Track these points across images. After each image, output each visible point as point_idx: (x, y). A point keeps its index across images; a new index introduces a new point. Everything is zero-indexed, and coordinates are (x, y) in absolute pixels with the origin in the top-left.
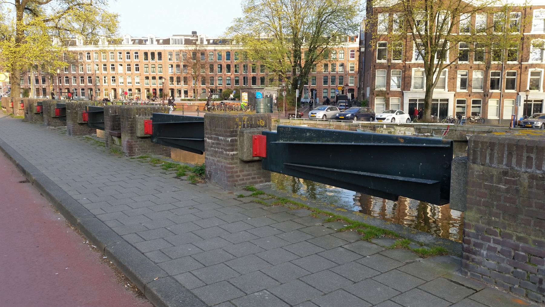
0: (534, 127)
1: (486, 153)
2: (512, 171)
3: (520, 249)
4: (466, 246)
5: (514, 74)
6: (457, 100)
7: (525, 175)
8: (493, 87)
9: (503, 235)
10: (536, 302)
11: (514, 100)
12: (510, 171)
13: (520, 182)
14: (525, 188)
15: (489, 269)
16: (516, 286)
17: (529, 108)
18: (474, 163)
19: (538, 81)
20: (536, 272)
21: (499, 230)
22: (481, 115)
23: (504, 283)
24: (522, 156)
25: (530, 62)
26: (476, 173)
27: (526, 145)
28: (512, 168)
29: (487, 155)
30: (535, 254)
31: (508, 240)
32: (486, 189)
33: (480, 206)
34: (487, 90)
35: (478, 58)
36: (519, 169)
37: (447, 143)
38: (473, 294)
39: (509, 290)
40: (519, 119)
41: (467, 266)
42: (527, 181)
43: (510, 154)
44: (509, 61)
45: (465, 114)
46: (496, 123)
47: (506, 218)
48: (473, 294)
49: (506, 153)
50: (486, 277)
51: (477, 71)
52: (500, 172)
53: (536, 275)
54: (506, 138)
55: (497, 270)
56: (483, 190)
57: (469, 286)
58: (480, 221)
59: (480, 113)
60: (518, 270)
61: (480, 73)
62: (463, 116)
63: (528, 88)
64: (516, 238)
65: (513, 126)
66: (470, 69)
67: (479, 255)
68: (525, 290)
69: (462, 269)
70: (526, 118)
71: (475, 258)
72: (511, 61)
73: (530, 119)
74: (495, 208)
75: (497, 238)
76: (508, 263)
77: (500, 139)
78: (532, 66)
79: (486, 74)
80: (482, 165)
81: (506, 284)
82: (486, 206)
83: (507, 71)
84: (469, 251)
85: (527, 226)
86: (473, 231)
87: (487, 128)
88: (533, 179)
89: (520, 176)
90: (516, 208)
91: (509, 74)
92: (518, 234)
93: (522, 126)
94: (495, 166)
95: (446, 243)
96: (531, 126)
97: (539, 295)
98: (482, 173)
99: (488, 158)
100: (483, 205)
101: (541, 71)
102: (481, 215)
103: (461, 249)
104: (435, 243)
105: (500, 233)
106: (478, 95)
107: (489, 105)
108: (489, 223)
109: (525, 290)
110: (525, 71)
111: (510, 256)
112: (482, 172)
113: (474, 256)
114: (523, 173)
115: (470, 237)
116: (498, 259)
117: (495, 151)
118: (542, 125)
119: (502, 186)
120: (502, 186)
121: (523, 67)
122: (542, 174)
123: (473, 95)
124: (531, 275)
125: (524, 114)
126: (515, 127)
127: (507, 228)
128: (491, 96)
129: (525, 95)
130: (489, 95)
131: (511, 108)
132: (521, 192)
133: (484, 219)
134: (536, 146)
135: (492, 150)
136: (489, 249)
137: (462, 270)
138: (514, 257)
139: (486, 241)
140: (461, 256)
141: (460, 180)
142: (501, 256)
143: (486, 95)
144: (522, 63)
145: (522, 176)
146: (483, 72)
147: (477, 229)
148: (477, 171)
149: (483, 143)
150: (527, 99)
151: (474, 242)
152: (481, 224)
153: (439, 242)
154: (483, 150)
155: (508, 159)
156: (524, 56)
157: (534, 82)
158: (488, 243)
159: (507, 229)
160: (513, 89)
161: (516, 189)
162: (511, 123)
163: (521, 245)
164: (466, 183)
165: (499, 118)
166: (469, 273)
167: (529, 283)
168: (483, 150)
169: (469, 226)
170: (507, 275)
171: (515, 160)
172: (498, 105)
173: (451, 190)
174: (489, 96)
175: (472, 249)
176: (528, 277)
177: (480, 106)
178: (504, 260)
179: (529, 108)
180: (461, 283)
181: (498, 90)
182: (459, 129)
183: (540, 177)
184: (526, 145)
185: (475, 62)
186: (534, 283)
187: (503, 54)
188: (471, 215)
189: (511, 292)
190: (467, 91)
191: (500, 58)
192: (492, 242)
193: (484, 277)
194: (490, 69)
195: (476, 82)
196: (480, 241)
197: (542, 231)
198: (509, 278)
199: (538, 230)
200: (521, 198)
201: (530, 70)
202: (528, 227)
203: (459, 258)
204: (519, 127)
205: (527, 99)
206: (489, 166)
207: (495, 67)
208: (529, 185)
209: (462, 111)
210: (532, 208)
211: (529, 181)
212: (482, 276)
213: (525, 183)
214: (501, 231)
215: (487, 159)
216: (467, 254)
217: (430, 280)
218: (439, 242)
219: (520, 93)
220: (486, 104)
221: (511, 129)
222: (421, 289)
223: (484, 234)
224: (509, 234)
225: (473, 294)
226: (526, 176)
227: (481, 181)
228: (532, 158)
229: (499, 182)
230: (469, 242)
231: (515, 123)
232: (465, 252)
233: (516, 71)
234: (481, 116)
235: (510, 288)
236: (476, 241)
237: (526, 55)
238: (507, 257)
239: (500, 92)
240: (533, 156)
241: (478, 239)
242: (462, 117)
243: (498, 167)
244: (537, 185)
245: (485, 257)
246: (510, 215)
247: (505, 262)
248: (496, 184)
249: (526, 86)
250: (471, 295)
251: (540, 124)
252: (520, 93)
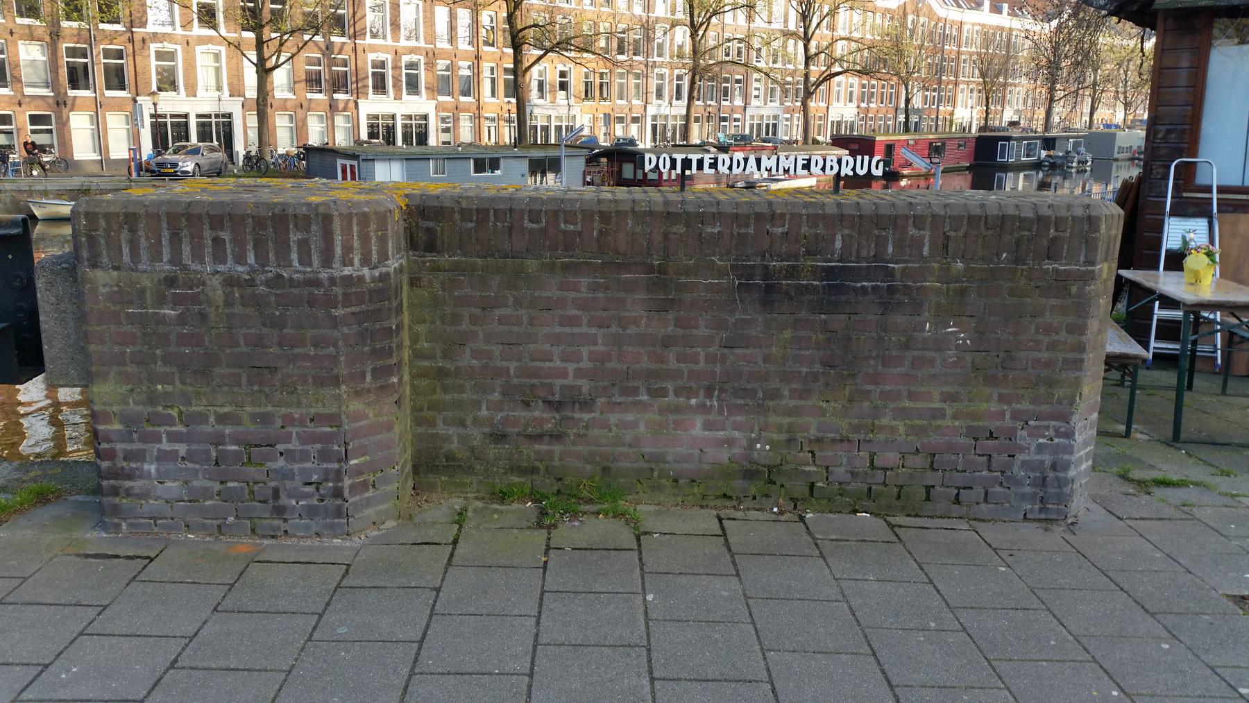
0: (179, 173)
1: (119, 241)
2: (186, 274)
3: (227, 439)
4: (105, 465)
5: (119, 55)
6: (30, 116)
7: (214, 280)
8: (74, 84)
9: (186, 419)
10: (273, 537)
11: (128, 113)
12: (181, 276)
13: (207, 295)
14: (218, 307)
15: (167, 502)
16: (231, 519)
17: (163, 131)
18: (95, 265)
19: (172, 71)
20: (264, 478)
21: (176, 410)
22: (56, 151)
23: (205, 521)
24: (201, 238)
25: (150, 28)
26: (102, 290)
27: (207, 213)
28: (185, 268)
29: (124, 245)
30: (258, 443)
31: (199, 428)
32: (132, 324)
33: (125, 364)
34: (62, 91)
35: (26, 9)
36: (199, 268)
37: (14, 224)
38: (145, 567)
39: (216, 533)
40: (145, 158)
41: (116, 510)
42: (220, 292)
43: (175, 238)
44: (103, 22)
45: (17, 149)
46: (96, 169)
47: (188, 380)
48: (145, 567)
49: (166, 235)
50: (165, 521)
51: (28, 42)
52: (159, 280)
53: (265, 484)
54: (159, 201)
55: (186, 499)
56: (127, 328)
57: (131, 554)
58: (131, 401)
59: (54, 147)
60: (230, 484)
61: (38, 47)
62: (10, 156)
63: (154, 88)
64: (215, 420)
65: (134, 174)
66: (9, 37)
67: (141, 477)
68: (249, 522)
69: (107, 520)
70: (159, 154)
71: (132, 488)
72: (108, 22)
73: (169, 157)
74: (159, 363)
75: (174, 429)
76: (207, 476)
77: (147, 203)
78: (155, 37)
79: (52, 51)
80: (115, 268)
81: (210, 521)
82: (138, 364)
83: (102, 47)
84: (116, 474)
85: (234, 388)
86: (116, 426)
87: (75, 182)
88: (232, 286)
89: (204, 284)
90: (206, 353)
91: (107, 53)
92: (218, 409)
93: (154, 172)
94: (145, 267)
95: (50, 469)
96: (172, 171)
97: (277, 522)
98: (116, 289)
99: (126, 251)
100: (131, 363)
101: (220, 51)
102: (130, 387)
103: (95, 474)
104: (20, 478)
105: (179, 417)
106: (40, 102)
107: (72, 127)
108: (152, 400)
109: (249, 522)
110: (143, 48)
111: (208, 459)
112: (118, 286)
113: (128, 484)
114: (211, 276)
115: (112, 442)
116: (183, 474)
117: (141, 233)
118: (194, 168)
119: (169, 312)
120: (169, 312)
121: (137, 38)
122: (248, 273)
123: (29, 102)
124: (256, 488)
125: (155, 146)
126: (139, 175)
127: (194, 402)
128: (73, 105)
129: (151, 103)
130: (69, 103)
131: (124, 133)
132: (212, 316)
133: (139, 394)
134: (229, 214)
135: (133, 231)
136: (163, 457)
137: (105, 523)
138: (216, 460)
139: (152, 443)
140: (98, 491)
141: (64, 312)
142: (190, 465)
143: (61, 103)
144: (134, 30)
145: (208, 283)
146: (45, 46)
147: (127, 420)
148: (104, 286)
149: (108, 216)
150: (156, 111)
151: (124, 450)
152: (133, 407)
153: (32, 474)
154: (112, 233)
155: (172, 250)
156: (136, 15)
157: (165, 74)
158: (157, 446)
159: (194, 405)
160: (121, 90)
161: (199, 313)
162: (129, 167)
163: (227, 431)
164: (82, 318)
165: (100, 158)
166: (124, 524)
167: (255, 503)
168: (112, 233)
169: (107, 418)
170: (208, 503)
171: (188, 249)
172: (128, 127)
173: (44, 341)
174: (69, 106)
175: (123, 468)
176: (252, 492)
177: (51, 129)
178: (196, 472)
179: (163, 131)
180: (110, 553)
181: (88, 91)
182: (7, 188)
183: (245, 280)
184: (207, 213)
185: (19, 20)
186: (265, 502)
187: (87, 4)
188: (107, 390)
189: (222, 534)
190: (12, 93)
191: (82, 15)
192: (164, 439)
193: (159, 522)
194: (61, 40)
195: (29, 70)
196: (137, 446)
197: (264, 392)
198: (213, 507)
199: (256, 391)
200: (213, 331)
201: (154, 47)
202: (235, 389)
203: (90, 498)
204: (148, 174)
205: (156, 111)
206: (133, 270)
207: (73, 35)
208: (225, 301)
209: (7, 143)
210: (239, 349)
211: (224, 292)
212: (155, 522)
213: (217, 298)
214: (181, 413)
215: (124, 254)
216: (112, 482)
217: (31, 573)
218: (32, 474)
219: (138, 98)
220: (64, 124)
221: (131, 181)
222: (13, 604)
223: (143, 427)
224: (199, 413)
225: (143, 569)
226: (216, 281)
227: (118, 308)
228: (224, 240)
229: (161, 301)
230: (111, 455)
231: (139, 168)
232: (108, 479)
233: (122, 48)
234: (57, 155)
235: (219, 526)
236: (129, 447)
237: (139, 12)
238: (203, 465)
239: (94, 95)
240: (225, 236)
241: (132, 441)
242: (8, 158)
243: (150, 272)
244: (242, 297)
245: (155, 479)
246: (195, 372)
247: (200, 477)
248: (154, 308)
249: (149, 83)
250: (140, 572)
251: (190, 167)
252: (138, 98)
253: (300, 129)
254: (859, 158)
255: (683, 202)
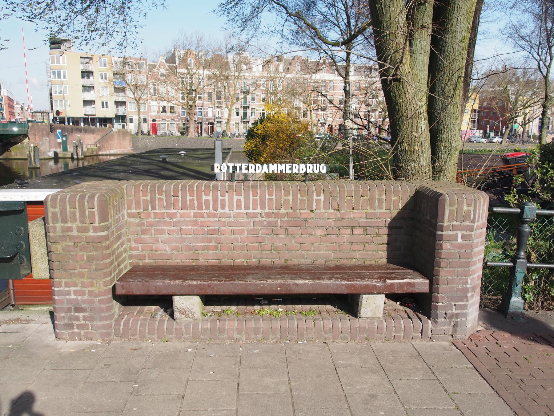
253: (83, 164)
254: (315, 165)
255: (58, 169)
